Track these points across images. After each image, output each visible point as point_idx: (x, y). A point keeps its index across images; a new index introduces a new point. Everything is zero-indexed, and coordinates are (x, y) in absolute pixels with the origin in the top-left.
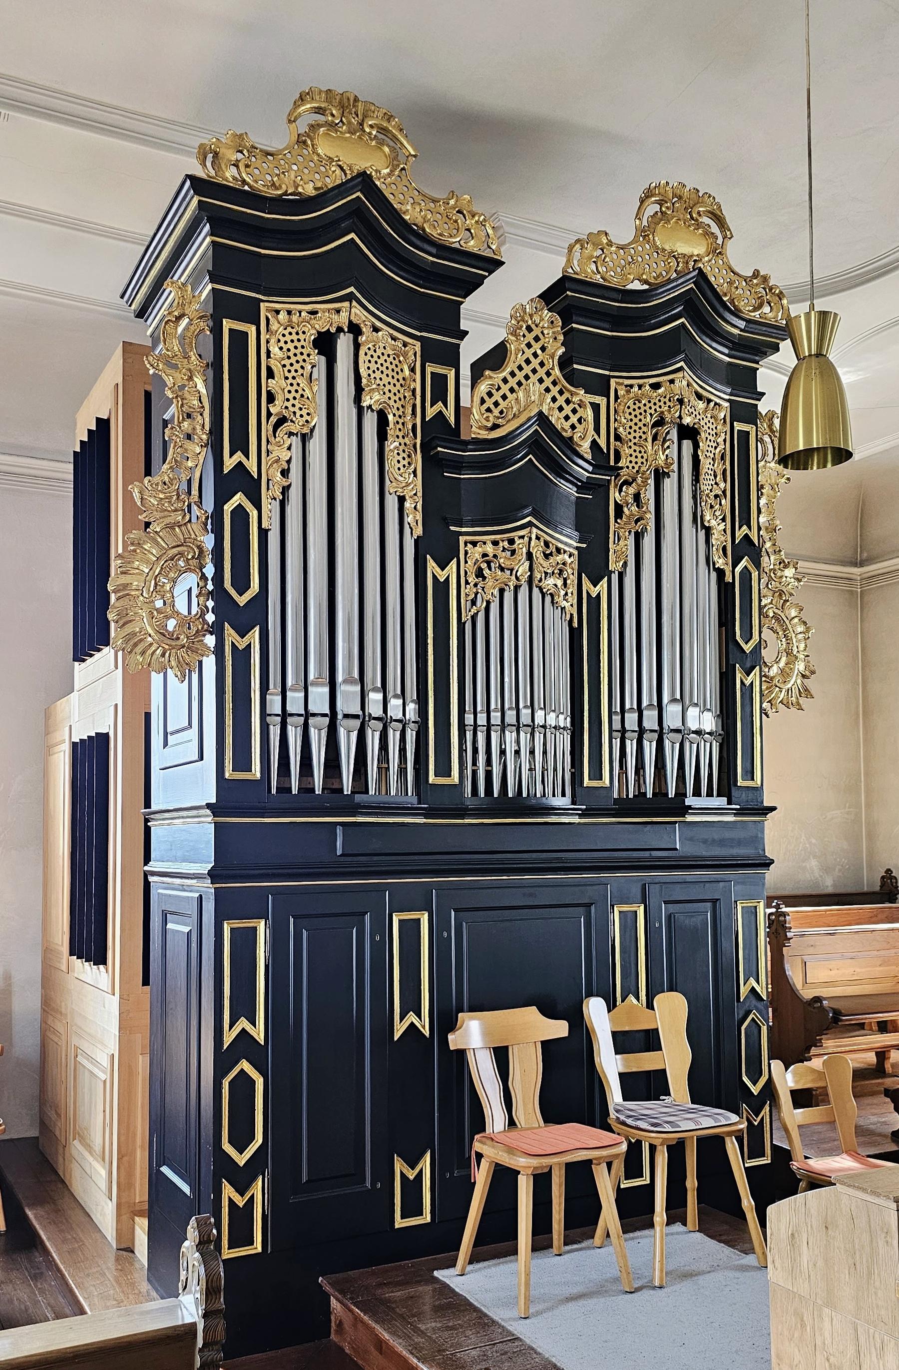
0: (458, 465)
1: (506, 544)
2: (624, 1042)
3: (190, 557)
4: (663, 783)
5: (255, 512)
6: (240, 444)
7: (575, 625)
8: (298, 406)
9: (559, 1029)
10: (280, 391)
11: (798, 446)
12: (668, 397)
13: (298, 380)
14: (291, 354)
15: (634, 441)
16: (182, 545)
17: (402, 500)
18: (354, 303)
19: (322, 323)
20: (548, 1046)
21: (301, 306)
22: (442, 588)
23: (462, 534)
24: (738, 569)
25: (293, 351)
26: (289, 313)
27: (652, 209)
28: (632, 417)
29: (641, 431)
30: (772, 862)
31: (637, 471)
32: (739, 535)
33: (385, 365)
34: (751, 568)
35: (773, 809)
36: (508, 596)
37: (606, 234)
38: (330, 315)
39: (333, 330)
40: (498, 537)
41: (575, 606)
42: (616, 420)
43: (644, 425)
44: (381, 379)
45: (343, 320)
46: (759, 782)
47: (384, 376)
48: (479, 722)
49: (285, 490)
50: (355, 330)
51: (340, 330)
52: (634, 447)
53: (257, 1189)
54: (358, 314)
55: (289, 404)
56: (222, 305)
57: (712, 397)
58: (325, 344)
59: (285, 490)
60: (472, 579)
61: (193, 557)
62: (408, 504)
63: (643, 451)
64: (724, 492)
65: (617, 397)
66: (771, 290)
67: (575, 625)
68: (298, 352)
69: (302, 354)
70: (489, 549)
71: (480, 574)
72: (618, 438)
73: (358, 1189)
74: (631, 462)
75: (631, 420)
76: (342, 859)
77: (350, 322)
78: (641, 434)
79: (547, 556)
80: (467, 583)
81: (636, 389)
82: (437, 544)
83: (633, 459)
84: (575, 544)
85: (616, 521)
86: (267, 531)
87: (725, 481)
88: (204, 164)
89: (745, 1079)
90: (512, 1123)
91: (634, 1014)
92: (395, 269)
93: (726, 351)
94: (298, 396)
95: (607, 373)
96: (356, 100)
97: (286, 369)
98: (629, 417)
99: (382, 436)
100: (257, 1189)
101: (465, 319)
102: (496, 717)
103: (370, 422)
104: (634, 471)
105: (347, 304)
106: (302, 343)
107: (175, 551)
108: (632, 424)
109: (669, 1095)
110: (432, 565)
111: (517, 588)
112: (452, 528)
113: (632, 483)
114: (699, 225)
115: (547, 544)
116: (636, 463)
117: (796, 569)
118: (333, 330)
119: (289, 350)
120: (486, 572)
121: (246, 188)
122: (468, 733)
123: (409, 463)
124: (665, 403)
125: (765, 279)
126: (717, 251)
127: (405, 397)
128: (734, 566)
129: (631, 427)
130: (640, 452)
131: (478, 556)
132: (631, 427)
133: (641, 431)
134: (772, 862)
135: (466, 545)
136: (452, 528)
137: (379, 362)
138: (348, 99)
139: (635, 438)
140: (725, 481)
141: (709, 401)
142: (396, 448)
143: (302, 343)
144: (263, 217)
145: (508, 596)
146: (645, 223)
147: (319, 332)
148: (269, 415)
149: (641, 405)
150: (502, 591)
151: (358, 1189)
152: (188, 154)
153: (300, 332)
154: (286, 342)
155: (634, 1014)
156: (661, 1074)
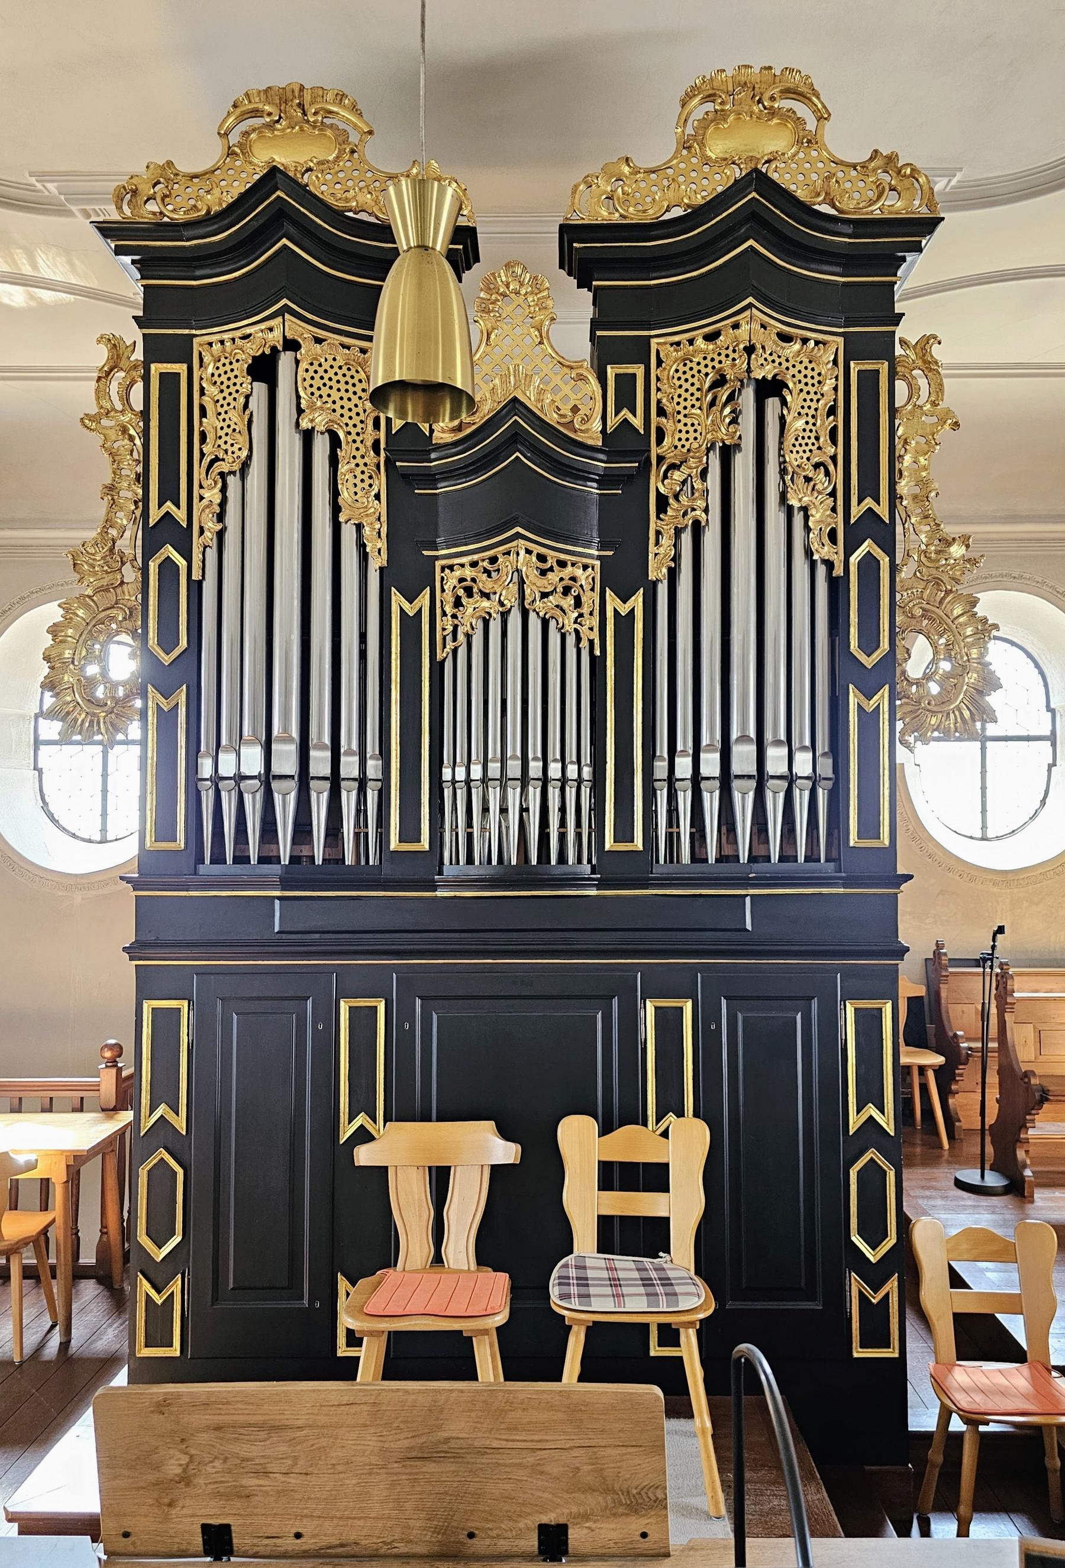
0: (430, 479)
1: (486, 564)
2: (615, 1176)
3: (120, 618)
4: (815, 841)
5: (184, 563)
6: (169, 492)
7: (597, 653)
8: (230, 442)
9: (507, 1152)
10: (212, 430)
11: (394, 377)
12: (731, 348)
13: (230, 414)
14: (224, 387)
15: (683, 412)
16: (113, 607)
17: (359, 527)
18: (287, 316)
19: (253, 349)
20: (498, 1172)
21: (227, 332)
22: (411, 624)
23: (437, 558)
24: (854, 559)
25: (226, 383)
26: (222, 342)
27: (699, 110)
28: (682, 382)
29: (694, 398)
30: (907, 949)
31: (689, 450)
32: (856, 512)
33: (335, 378)
34: (878, 553)
35: (910, 877)
36: (495, 627)
37: (627, 159)
38: (263, 333)
39: (268, 351)
40: (475, 557)
41: (596, 629)
42: (658, 390)
43: (698, 390)
44: (329, 396)
45: (275, 338)
46: (887, 842)
47: (333, 392)
48: (705, 771)
49: (221, 535)
50: (292, 345)
51: (274, 349)
52: (684, 420)
53: (176, 1286)
54: (295, 328)
55: (221, 442)
56: (155, 349)
57: (809, 334)
58: (263, 369)
59: (221, 535)
60: (449, 609)
61: (125, 619)
62: (367, 531)
63: (696, 422)
64: (834, 458)
65: (660, 362)
66: (899, 172)
67: (597, 653)
68: (231, 383)
69: (235, 384)
70: (468, 573)
71: (458, 603)
72: (661, 412)
73: (296, 1304)
74: (680, 440)
75: (680, 386)
76: (278, 936)
77: (284, 337)
78: (694, 402)
79: (543, 573)
80: (444, 614)
81: (812, 343)
82: (408, 572)
83: (683, 436)
84: (596, 553)
85: (658, 517)
86: (200, 583)
87: (834, 442)
88: (119, 208)
89: (856, 1239)
90: (438, 1259)
91: (632, 1144)
92: (663, 274)
93: (838, 269)
94: (230, 431)
95: (186, 332)
96: (302, 88)
97: (219, 405)
98: (678, 383)
99: (334, 462)
100: (176, 1286)
101: (138, 304)
102: (494, 769)
103: (321, 448)
104: (685, 450)
105: (280, 319)
106: (235, 373)
107: (103, 614)
108: (681, 391)
109: (669, 1252)
110: (397, 600)
111: (505, 616)
112: (425, 553)
113: (680, 466)
114: (773, 113)
115: (542, 558)
116: (687, 440)
117: (968, 546)
118: (268, 351)
119: (222, 383)
120: (464, 600)
121: (166, 219)
122: (446, 791)
123: (371, 485)
124: (727, 356)
125: (891, 159)
126: (809, 141)
127: (365, 411)
128: (848, 554)
129: (680, 396)
130: (693, 425)
131: (455, 582)
132: (680, 396)
133: (694, 398)
134: (907, 949)
135: (443, 570)
136: (425, 553)
137: (326, 376)
138: (293, 91)
139: (685, 408)
140: (834, 442)
141: (805, 341)
142: (351, 471)
143: (235, 373)
144: (184, 247)
145: (495, 627)
146: (689, 130)
147: (254, 358)
148: (202, 455)
149: (694, 365)
150: (486, 623)
151: (296, 1304)
152: (104, 201)
153: (234, 361)
154: (812, 377)
155: (632, 1144)
156: (662, 1225)
